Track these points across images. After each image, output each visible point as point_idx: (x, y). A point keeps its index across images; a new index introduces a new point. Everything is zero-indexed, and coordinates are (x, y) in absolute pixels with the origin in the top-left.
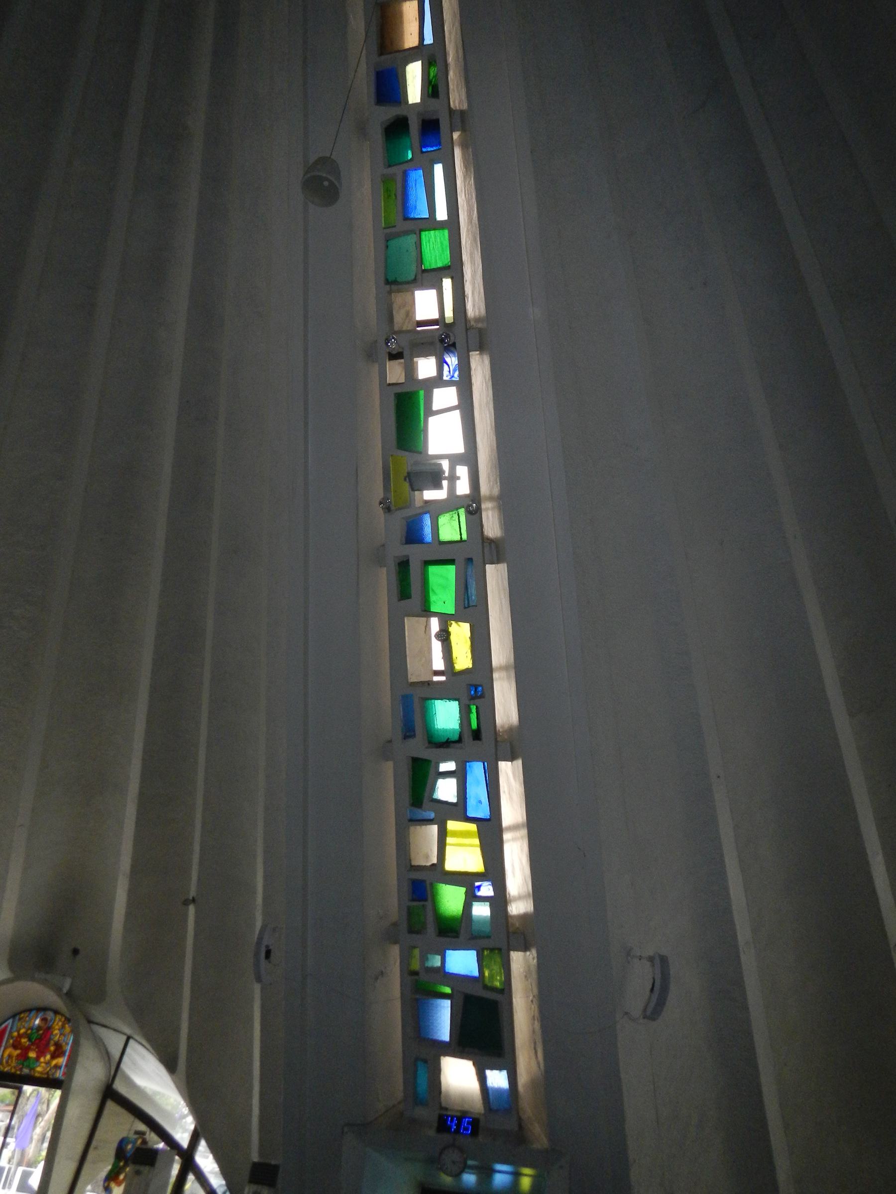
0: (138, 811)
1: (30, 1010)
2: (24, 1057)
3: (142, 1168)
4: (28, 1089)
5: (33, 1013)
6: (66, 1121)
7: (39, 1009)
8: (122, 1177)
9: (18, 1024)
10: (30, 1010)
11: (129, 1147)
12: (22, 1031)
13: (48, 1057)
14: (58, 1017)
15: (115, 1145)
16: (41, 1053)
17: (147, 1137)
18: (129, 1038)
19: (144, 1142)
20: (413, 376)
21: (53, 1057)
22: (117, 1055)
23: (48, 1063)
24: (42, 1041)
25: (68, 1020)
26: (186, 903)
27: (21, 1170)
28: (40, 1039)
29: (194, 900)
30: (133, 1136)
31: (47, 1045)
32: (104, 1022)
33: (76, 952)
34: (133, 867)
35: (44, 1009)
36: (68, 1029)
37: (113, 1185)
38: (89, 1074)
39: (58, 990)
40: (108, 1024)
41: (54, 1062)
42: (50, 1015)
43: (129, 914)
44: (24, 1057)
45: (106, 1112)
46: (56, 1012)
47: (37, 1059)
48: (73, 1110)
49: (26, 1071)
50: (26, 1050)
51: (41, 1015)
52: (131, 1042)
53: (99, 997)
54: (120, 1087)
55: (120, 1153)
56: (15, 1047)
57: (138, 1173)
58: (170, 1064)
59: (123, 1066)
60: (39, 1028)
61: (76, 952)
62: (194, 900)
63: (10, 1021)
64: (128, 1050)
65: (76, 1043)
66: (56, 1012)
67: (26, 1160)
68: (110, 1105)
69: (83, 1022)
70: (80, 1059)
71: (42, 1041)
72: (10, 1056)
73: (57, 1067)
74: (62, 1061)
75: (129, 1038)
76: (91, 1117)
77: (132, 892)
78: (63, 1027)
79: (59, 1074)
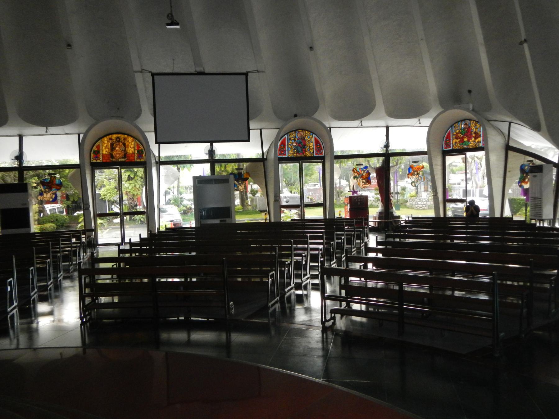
0: (478, 9)
1: (458, 122)
2: (462, 141)
3: (536, 174)
4: (469, 154)
5: (460, 123)
6: (491, 163)
7: (462, 121)
8: (527, 180)
9: (454, 129)
10: (458, 122)
11: (526, 167)
12: (457, 131)
13: (473, 139)
14: (472, 122)
15: (519, 169)
16: (470, 138)
17: (534, 161)
18: (510, 123)
19: (533, 164)
20: (76, 356)
21: (476, 138)
22: (507, 133)
23: (474, 141)
24: (468, 133)
25: (478, 122)
26: (521, 43)
27: (478, 190)
28: (467, 132)
29: (525, 41)
30: (526, 163)
31: (471, 134)
32: (494, 118)
33: (470, 92)
34: (485, 39)
35: (464, 120)
36: (478, 125)
37: (523, 184)
38: (495, 142)
39: (468, 110)
40: (497, 119)
41: (477, 141)
42: (468, 122)
43: (490, 64)
44: (462, 141)
45: (509, 160)
46: (470, 120)
47: (469, 141)
48: (493, 158)
49: (465, 147)
50: (462, 138)
51: (463, 123)
52: (512, 124)
53: (488, 107)
54: (511, 144)
55: (522, 170)
56: (457, 138)
57: (535, 176)
58: (536, 128)
59: (511, 136)
60: (465, 128)
61: (470, 92)
62: (525, 41)
63: (450, 129)
64: (511, 129)
65: (485, 130)
66: (470, 120)
67: (479, 186)
68: (510, 153)
69: (485, 122)
70: (488, 136)
71: (468, 133)
72: (456, 142)
73: (479, 142)
74: (480, 139)
75: (510, 123)
76: (503, 164)
77: (488, 52)
78: (476, 125)
79: (481, 145)
